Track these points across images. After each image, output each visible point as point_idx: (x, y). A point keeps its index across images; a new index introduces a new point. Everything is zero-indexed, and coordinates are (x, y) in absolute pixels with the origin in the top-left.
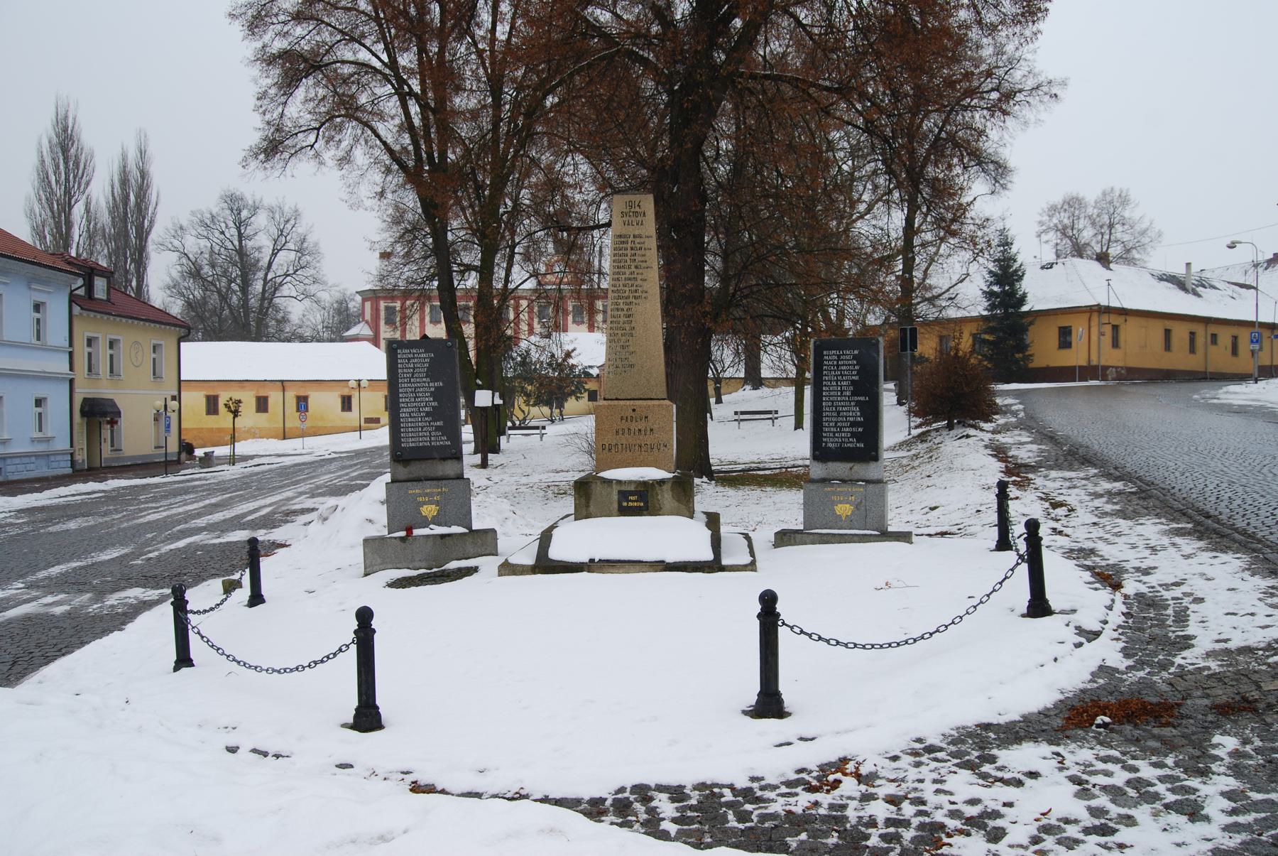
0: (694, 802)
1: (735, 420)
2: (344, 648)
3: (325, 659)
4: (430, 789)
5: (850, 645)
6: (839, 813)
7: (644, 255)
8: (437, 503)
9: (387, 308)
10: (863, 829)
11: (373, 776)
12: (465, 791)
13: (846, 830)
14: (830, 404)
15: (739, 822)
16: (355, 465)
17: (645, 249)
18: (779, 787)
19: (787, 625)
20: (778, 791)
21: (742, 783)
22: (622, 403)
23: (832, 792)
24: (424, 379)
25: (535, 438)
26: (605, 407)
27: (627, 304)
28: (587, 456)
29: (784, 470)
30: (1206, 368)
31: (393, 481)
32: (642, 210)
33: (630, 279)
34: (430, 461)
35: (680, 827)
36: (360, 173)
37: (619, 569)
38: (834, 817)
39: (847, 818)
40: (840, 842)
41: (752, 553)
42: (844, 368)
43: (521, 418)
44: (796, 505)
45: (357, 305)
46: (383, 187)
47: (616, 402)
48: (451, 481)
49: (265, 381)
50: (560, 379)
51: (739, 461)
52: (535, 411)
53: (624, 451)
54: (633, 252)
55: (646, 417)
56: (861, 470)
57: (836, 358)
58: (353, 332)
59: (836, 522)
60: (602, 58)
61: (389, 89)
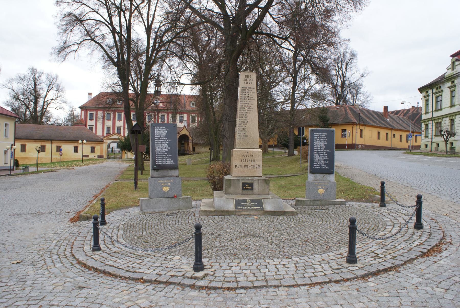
8: (169, 186)
9: (90, 114)
14: (316, 152)
27: (245, 113)
30: (391, 144)
33: (246, 104)
42: (322, 139)
54: (248, 94)
57: (319, 136)
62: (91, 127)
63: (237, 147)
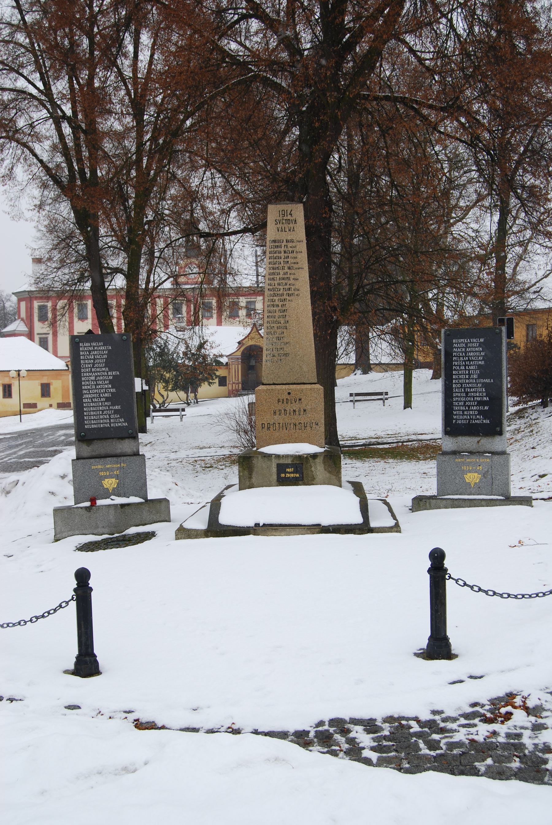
0: (386, 733)
1: (351, 401)
2: (64, 605)
3: (46, 614)
4: (151, 726)
5: (519, 596)
6: (516, 741)
7: (295, 258)
8: (117, 477)
10: (540, 754)
11: (99, 715)
12: (183, 727)
13: (525, 755)
14: (459, 386)
15: (430, 750)
16: (21, 445)
17: (297, 252)
18: (458, 719)
19: (453, 579)
20: (458, 723)
21: (425, 716)
22: (278, 387)
23: (506, 723)
24: (103, 369)
25: (174, 420)
26: (263, 391)
28: (235, 434)
29: (400, 444)
31: (78, 458)
32: (294, 218)
33: (283, 279)
34: (110, 440)
35: (379, 755)
36: (20, 187)
37: (281, 531)
38: (513, 744)
39: (524, 745)
40: (523, 766)
41: (394, 517)
42: (472, 354)
43: (161, 402)
44: (417, 474)
45: (13, 305)
46: (41, 201)
47: (273, 387)
48: (128, 457)
49: (53, 370)
50: (194, 368)
51: (358, 436)
52: (173, 395)
53: (281, 430)
54: (286, 255)
55: (300, 400)
56: (489, 443)
57: (464, 345)
58: (10, 328)
59: (466, 488)
60: (239, 83)
61: (44, 113)
62: (44, 338)
63: (265, 382)
